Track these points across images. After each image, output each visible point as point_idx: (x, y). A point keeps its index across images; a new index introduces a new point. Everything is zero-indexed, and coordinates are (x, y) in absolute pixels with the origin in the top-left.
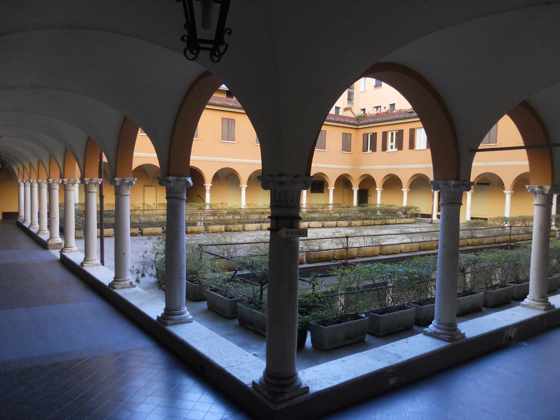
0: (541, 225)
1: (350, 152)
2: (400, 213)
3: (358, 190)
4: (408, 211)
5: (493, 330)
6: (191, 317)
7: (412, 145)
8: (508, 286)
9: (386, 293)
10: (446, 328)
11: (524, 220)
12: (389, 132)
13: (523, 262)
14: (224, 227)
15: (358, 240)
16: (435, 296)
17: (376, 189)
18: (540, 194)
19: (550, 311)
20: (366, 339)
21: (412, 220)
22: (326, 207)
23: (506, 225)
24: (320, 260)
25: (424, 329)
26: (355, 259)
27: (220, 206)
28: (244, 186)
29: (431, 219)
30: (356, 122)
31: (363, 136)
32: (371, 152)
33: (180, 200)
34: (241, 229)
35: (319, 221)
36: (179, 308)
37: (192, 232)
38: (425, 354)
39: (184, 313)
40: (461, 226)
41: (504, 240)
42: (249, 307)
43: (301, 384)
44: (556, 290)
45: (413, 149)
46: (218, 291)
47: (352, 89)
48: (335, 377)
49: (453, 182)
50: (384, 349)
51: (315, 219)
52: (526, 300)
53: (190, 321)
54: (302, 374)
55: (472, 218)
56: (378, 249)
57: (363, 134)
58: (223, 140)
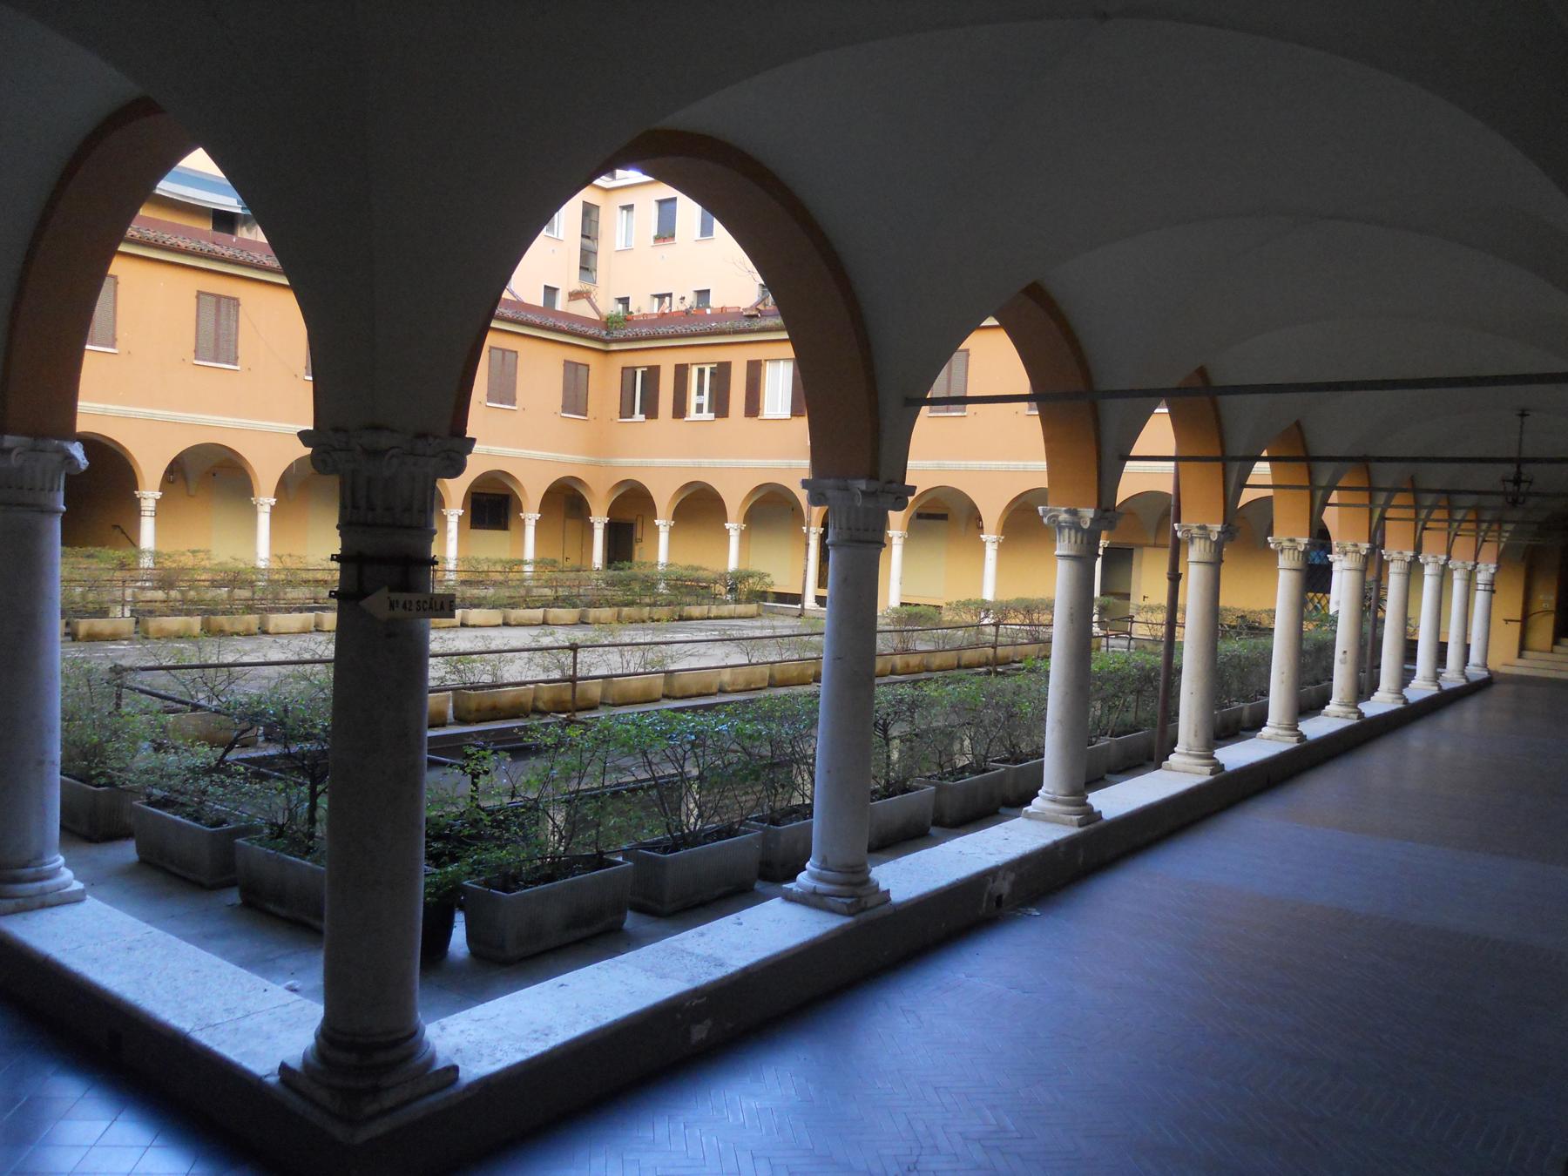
0: (1071, 608)
1: (586, 415)
2: (720, 588)
3: (605, 524)
4: (740, 582)
5: (958, 880)
6: (77, 886)
7: (753, 407)
8: (994, 770)
9: (681, 794)
10: (839, 877)
11: (1028, 608)
12: (693, 366)
13: (1027, 708)
14: (199, 622)
15: (604, 657)
16: (812, 800)
17: (657, 522)
18: (1070, 529)
19: (1091, 826)
20: (625, 924)
21: (752, 608)
22: (516, 568)
23: (986, 621)
24: (495, 713)
25: (785, 886)
26: (595, 711)
27: (188, 561)
28: (265, 501)
29: (799, 606)
30: (604, 333)
31: (622, 373)
32: (644, 419)
33: (42, 512)
34: (255, 628)
35: (493, 608)
36: (36, 859)
37: (93, 637)
38: (787, 951)
39: (55, 873)
40: (881, 623)
41: (981, 660)
42: (273, 849)
43: (432, 1059)
44: (1102, 779)
45: (757, 416)
46: (172, 807)
47: (593, 241)
48: (536, 1032)
49: (862, 485)
50: (677, 944)
51: (484, 602)
52: (1034, 801)
53: (75, 899)
54: (439, 1031)
55: (902, 604)
56: (659, 680)
57: (623, 368)
58: (199, 359)
